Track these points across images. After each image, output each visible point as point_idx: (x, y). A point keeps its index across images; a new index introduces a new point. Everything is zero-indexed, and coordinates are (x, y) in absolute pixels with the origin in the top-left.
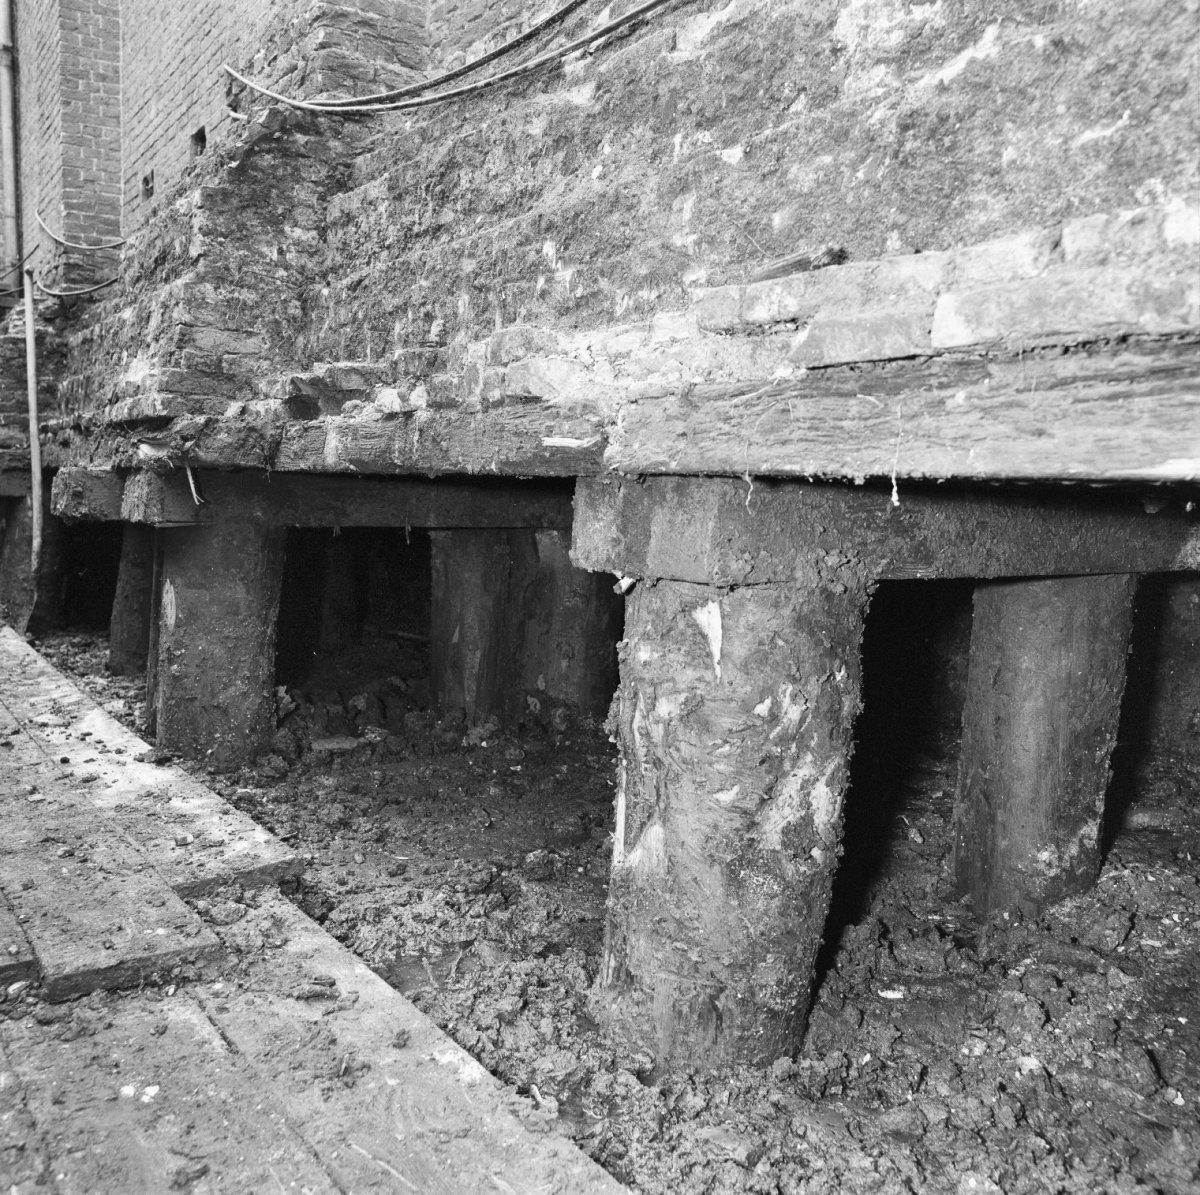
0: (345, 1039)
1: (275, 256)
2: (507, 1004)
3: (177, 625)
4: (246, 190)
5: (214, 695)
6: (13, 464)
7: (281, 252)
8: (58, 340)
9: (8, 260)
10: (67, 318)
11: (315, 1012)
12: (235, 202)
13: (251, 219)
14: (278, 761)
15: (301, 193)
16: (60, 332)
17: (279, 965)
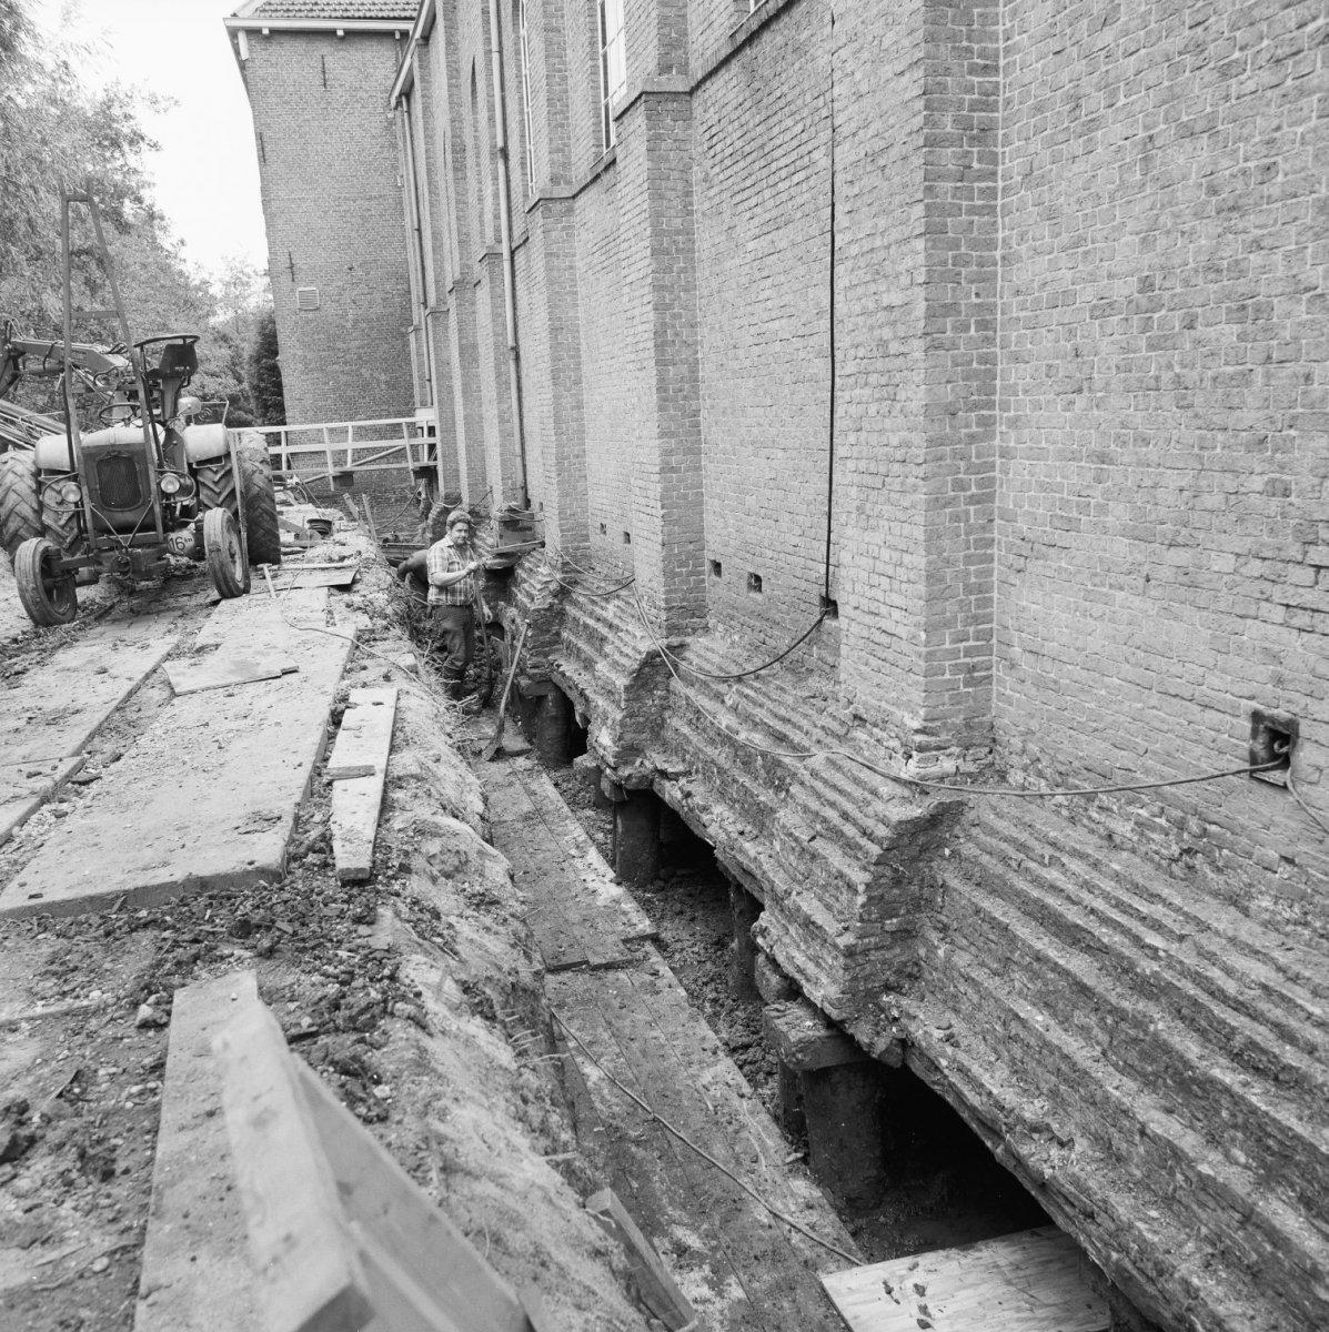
9: (520, 483)
14: (661, 883)
15: (659, 679)
17: (647, 965)
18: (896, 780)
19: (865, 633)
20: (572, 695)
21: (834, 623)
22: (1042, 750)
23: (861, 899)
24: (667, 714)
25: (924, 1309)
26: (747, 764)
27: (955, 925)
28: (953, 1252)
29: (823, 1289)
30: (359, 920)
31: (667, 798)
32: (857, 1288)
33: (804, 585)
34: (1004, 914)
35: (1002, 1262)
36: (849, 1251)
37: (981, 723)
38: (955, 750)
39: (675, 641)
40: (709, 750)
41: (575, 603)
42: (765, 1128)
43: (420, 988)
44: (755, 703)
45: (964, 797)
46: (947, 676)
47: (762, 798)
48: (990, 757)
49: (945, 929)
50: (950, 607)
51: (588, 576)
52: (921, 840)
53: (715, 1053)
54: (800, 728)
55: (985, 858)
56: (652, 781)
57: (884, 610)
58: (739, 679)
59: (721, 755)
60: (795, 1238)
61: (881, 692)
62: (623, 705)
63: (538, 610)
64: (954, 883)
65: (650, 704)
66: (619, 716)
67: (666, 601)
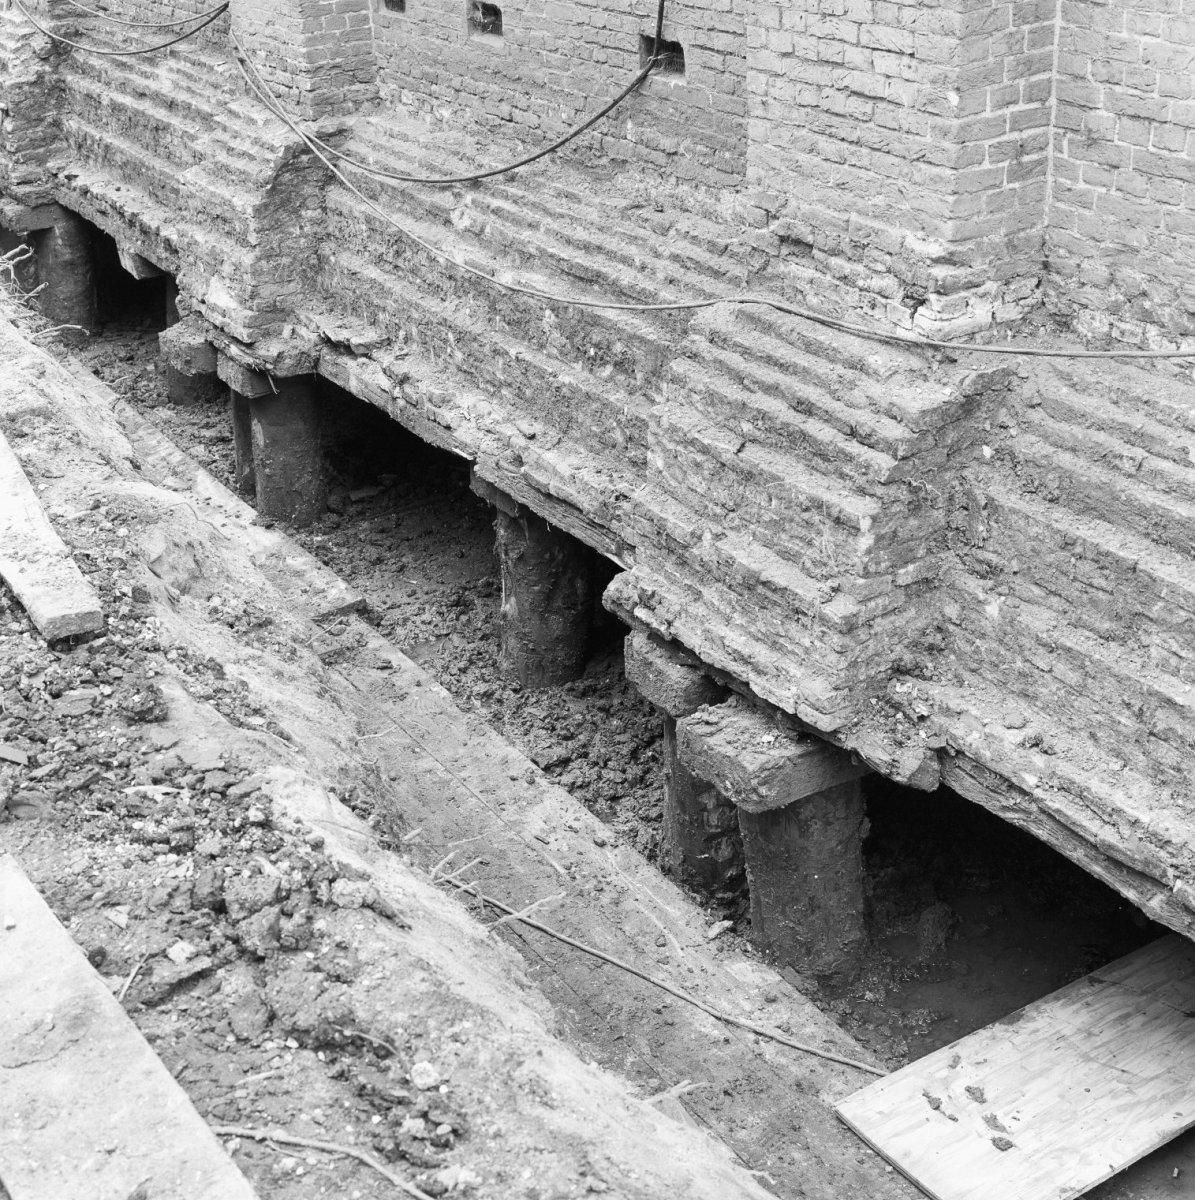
0: (398, 684)
1: (298, 232)
2: (462, 665)
3: (266, 446)
4: (277, 200)
5: (292, 484)
6: (40, 201)
7: (301, 228)
8: (55, 77)
10: (60, 54)
11: (385, 674)
12: (272, 208)
13: (283, 216)
14: (334, 517)
15: (307, 190)
16: (55, 70)
18: (890, 342)
19: (809, 97)
20: (109, 225)
21: (674, 81)
22: (1152, 278)
23: (865, 541)
24: (327, 248)
25: (992, 1121)
26: (520, 323)
27: (1015, 565)
28: (998, 1029)
29: (840, 1120)
30: (141, 717)
31: (353, 386)
32: (899, 1107)
33: (601, 18)
34: (1123, 546)
35: (1067, 1032)
36: (853, 1054)
37: (1028, 240)
38: (991, 286)
39: (329, 124)
40: (432, 304)
41: (85, 70)
42: (656, 888)
43: (318, 833)
44: (517, 222)
45: (1011, 362)
46: (987, 165)
47: (564, 379)
48: (1038, 293)
49: (991, 572)
50: (995, 44)
51: (102, 24)
52: (951, 437)
53: (532, 782)
54: (626, 261)
55: (1065, 459)
56: (317, 361)
57: (855, 56)
58: (475, 183)
59: (463, 313)
60: (769, 1050)
61: (848, 197)
62: (253, 239)
63: (19, 86)
64: (1007, 496)
65: (298, 233)
66: (247, 258)
67: (309, 57)
